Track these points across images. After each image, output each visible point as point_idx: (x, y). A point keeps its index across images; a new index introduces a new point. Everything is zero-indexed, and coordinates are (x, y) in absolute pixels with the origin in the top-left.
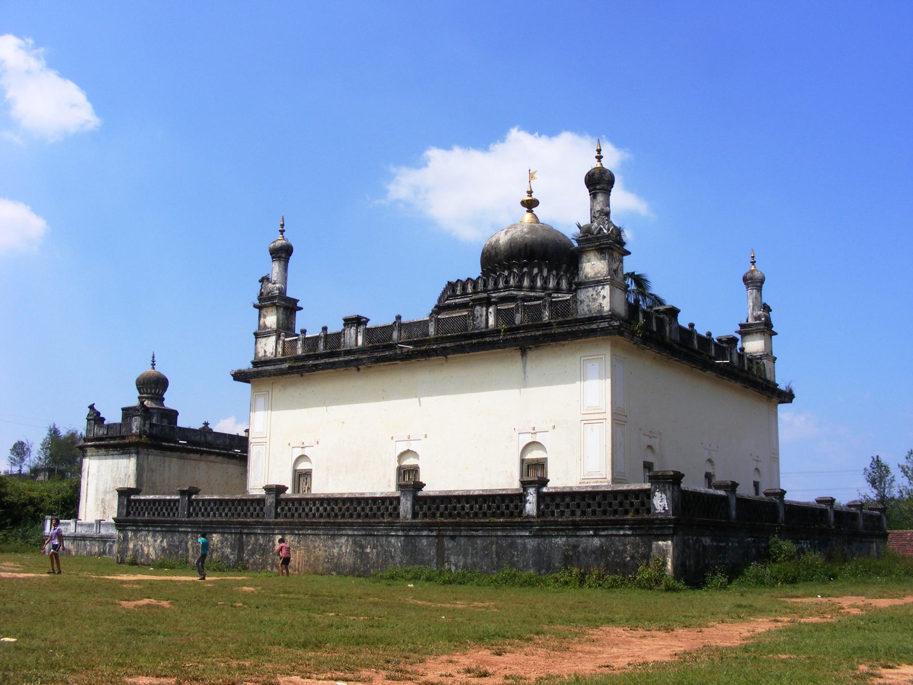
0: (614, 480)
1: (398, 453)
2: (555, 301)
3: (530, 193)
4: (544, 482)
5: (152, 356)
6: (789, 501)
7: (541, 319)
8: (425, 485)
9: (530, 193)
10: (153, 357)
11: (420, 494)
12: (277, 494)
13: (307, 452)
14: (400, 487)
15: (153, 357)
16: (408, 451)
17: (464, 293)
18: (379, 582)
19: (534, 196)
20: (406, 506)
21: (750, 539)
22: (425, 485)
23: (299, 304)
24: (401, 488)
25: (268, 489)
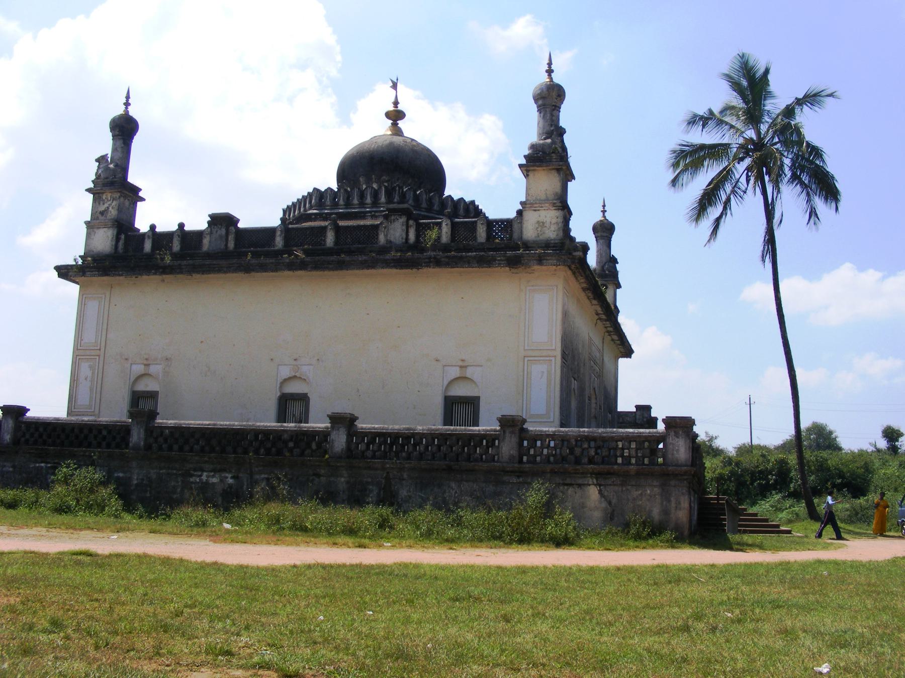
0: (69, 414)
1: (280, 380)
2: (348, 227)
3: (396, 103)
4: (153, 415)
5: (602, 204)
6: (756, 444)
7: (475, 238)
8: (29, 410)
9: (396, 103)
10: (604, 206)
11: (21, 419)
12: (17, 418)
13: (469, 373)
14: (131, 415)
15: (604, 206)
16: (295, 377)
17: (335, 205)
18: (116, 517)
19: (400, 107)
20: (137, 436)
21: (43, 465)
22: (29, 410)
23: (141, 194)
24: (522, 421)
25: (337, 420)
